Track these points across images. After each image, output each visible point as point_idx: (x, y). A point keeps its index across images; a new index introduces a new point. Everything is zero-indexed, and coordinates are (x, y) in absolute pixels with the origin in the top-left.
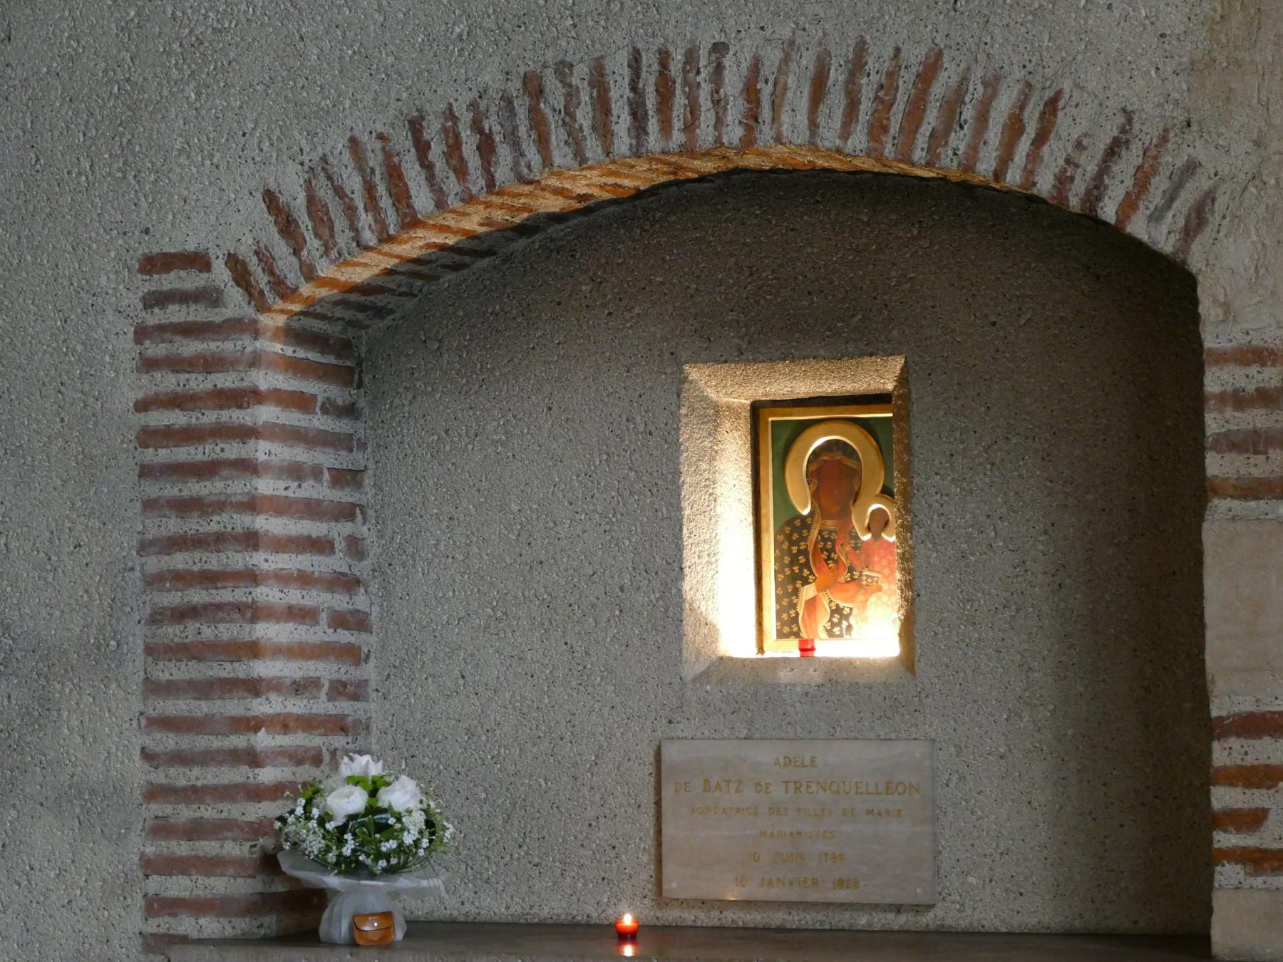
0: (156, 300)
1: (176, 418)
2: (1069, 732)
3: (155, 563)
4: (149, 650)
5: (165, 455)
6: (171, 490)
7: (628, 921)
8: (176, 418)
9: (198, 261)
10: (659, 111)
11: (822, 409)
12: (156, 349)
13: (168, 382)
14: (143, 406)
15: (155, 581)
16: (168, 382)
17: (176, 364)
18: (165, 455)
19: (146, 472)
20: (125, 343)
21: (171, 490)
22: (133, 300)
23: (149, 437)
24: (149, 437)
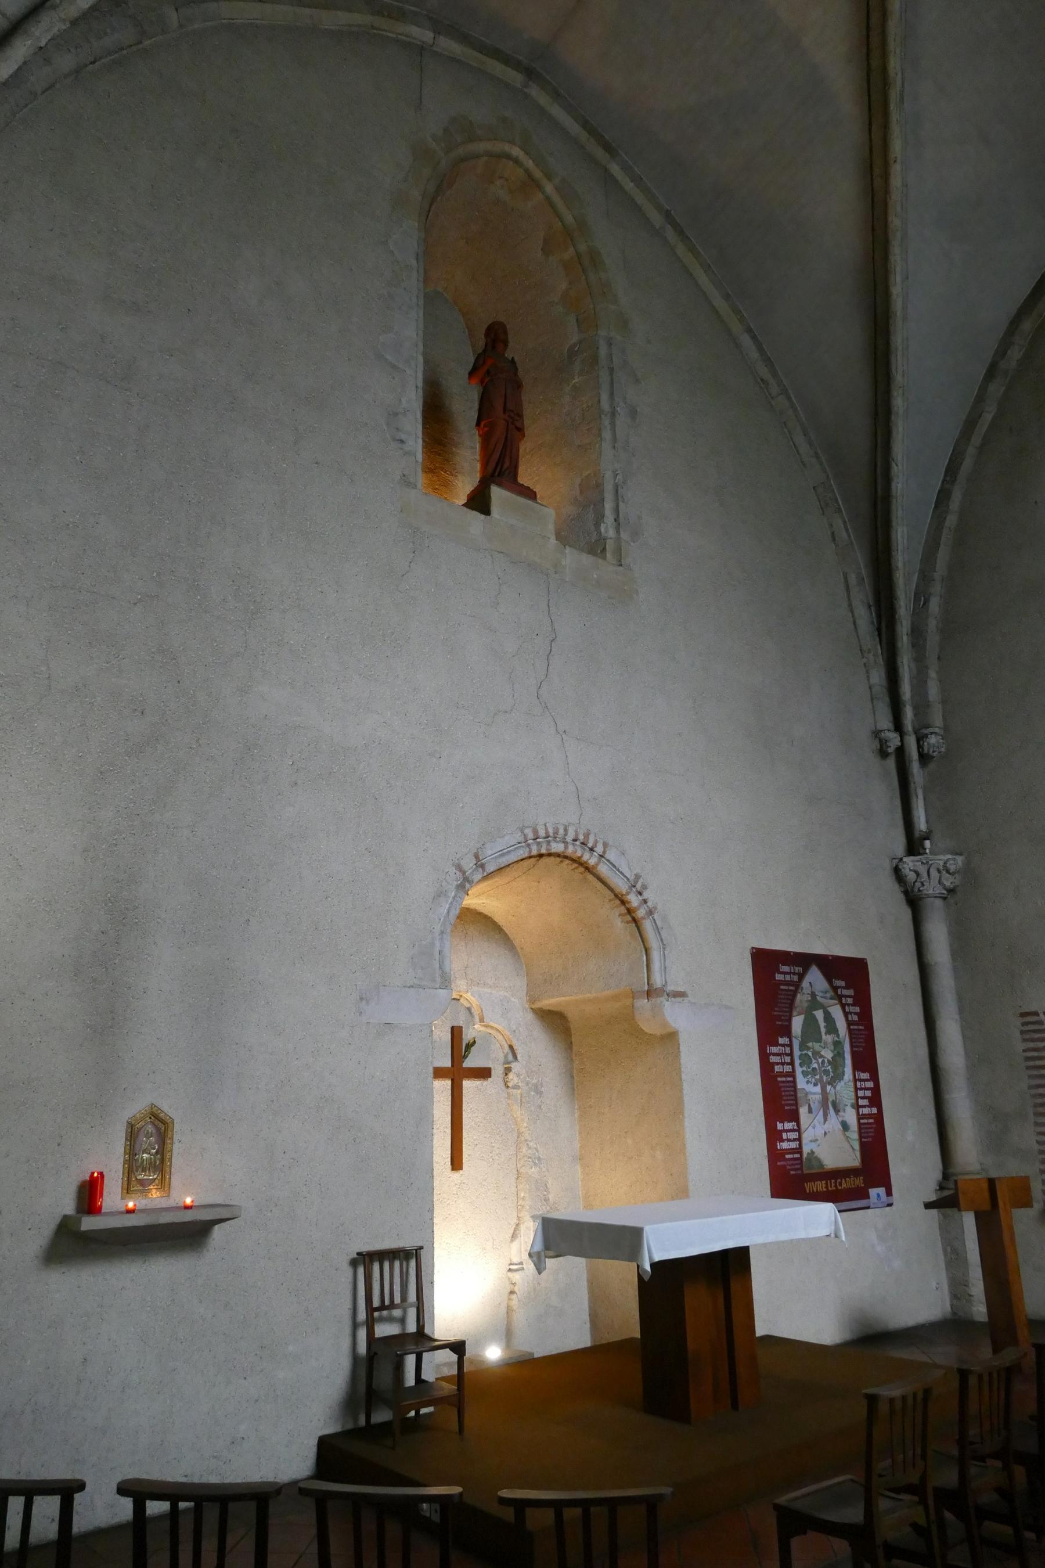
0: (1024, 1024)
1: (1035, 1054)
2: (306, 1442)
3: (1034, 1091)
4: (1035, 1114)
5: (1032, 1063)
6: (1035, 1072)
7: (188, 1201)
8: (1035, 1054)
9: (1036, 1014)
10: (928, 705)
11: (914, 800)
12: (1027, 1036)
13: (1031, 1045)
14: (1024, 1051)
15: (1034, 1096)
16: (1031, 1045)
17: (1033, 1040)
18: (1032, 1063)
19: (1028, 1068)
20: (1018, 1034)
21: (1035, 1072)
22: (1019, 1024)
23: (1028, 1059)
24: (1028, 1059)
